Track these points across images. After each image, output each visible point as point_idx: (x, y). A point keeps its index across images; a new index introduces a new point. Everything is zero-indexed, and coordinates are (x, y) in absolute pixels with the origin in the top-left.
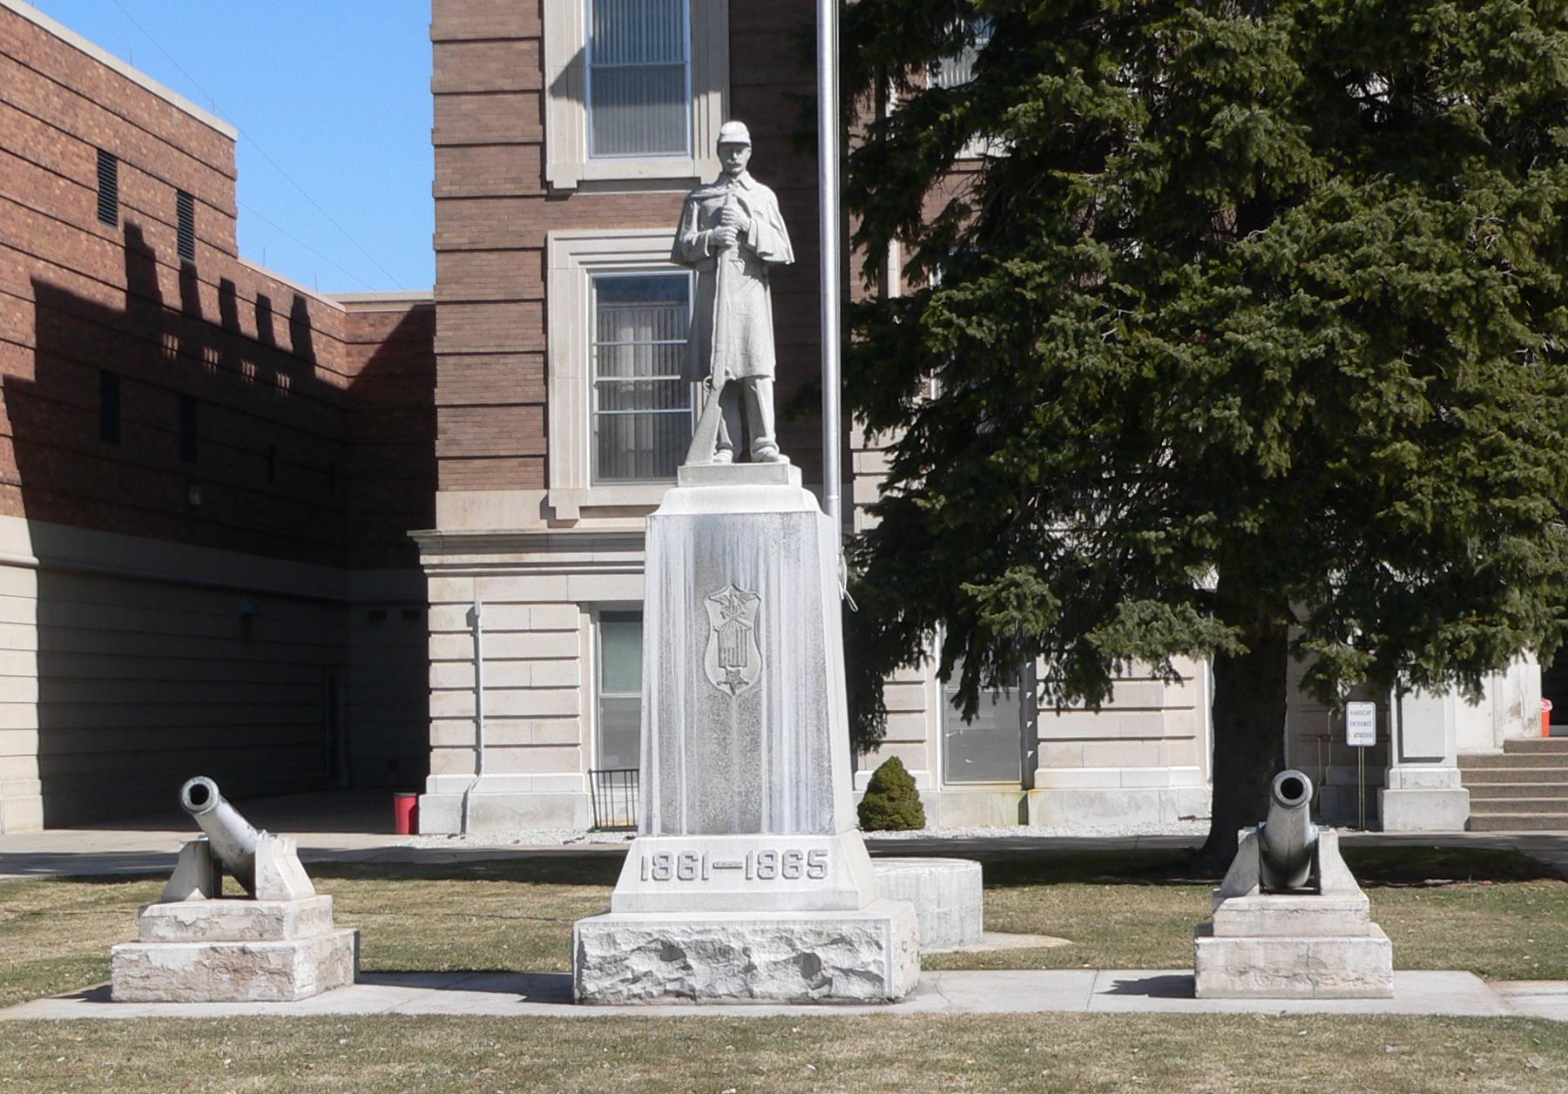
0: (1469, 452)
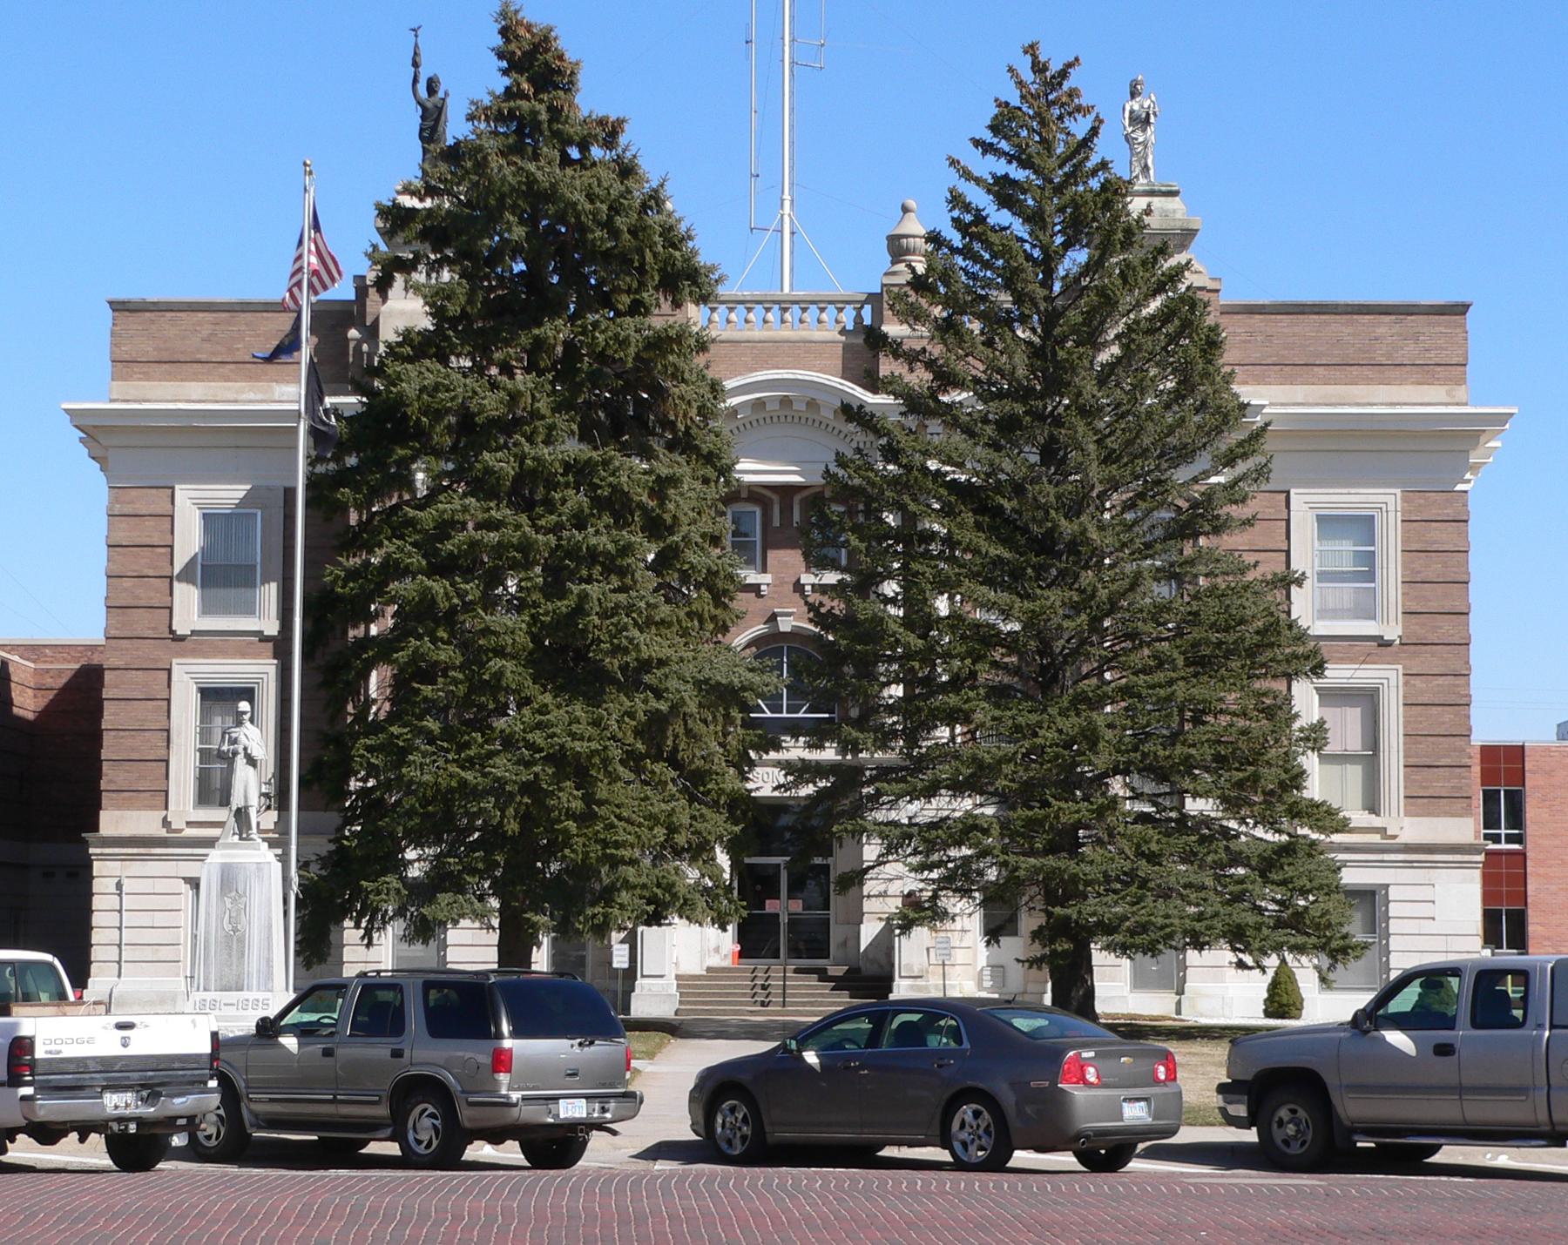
0: (599, 827)
